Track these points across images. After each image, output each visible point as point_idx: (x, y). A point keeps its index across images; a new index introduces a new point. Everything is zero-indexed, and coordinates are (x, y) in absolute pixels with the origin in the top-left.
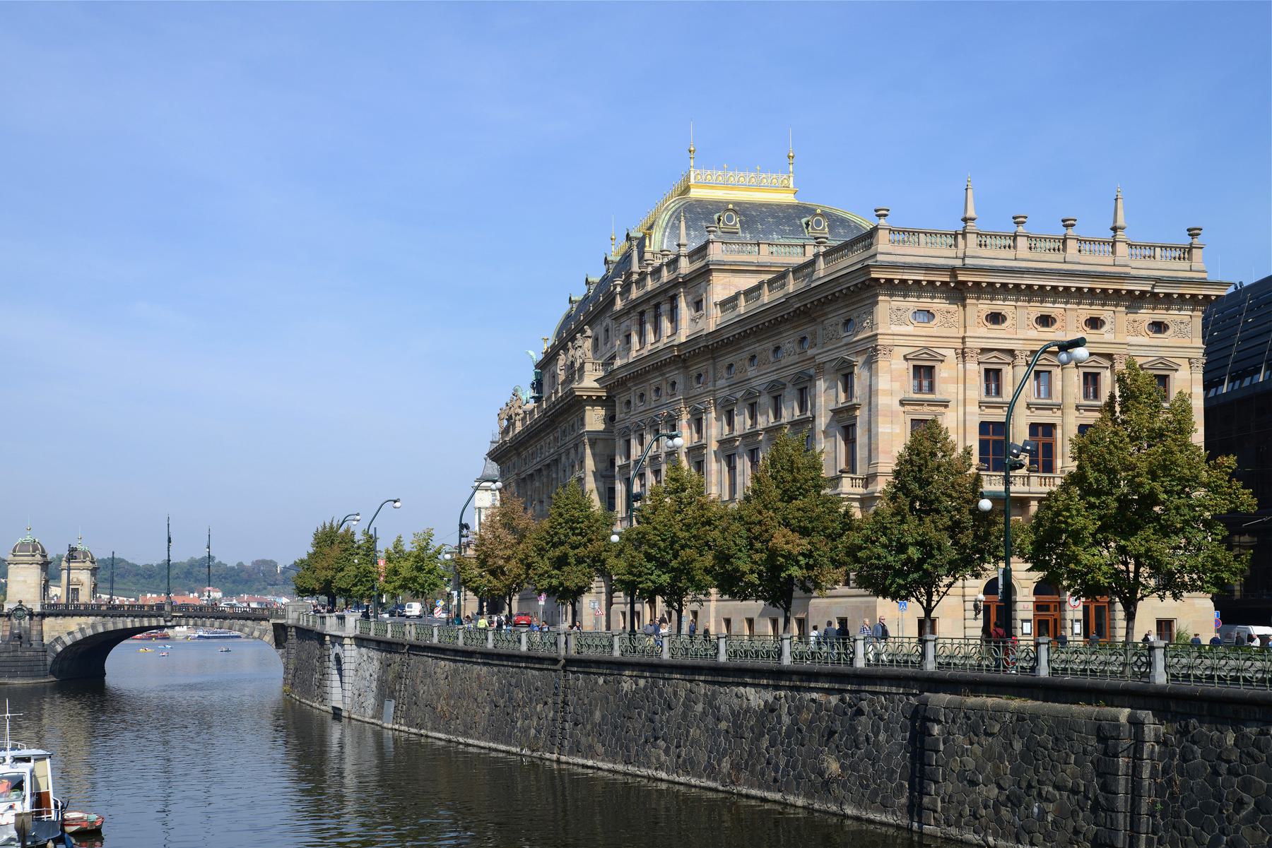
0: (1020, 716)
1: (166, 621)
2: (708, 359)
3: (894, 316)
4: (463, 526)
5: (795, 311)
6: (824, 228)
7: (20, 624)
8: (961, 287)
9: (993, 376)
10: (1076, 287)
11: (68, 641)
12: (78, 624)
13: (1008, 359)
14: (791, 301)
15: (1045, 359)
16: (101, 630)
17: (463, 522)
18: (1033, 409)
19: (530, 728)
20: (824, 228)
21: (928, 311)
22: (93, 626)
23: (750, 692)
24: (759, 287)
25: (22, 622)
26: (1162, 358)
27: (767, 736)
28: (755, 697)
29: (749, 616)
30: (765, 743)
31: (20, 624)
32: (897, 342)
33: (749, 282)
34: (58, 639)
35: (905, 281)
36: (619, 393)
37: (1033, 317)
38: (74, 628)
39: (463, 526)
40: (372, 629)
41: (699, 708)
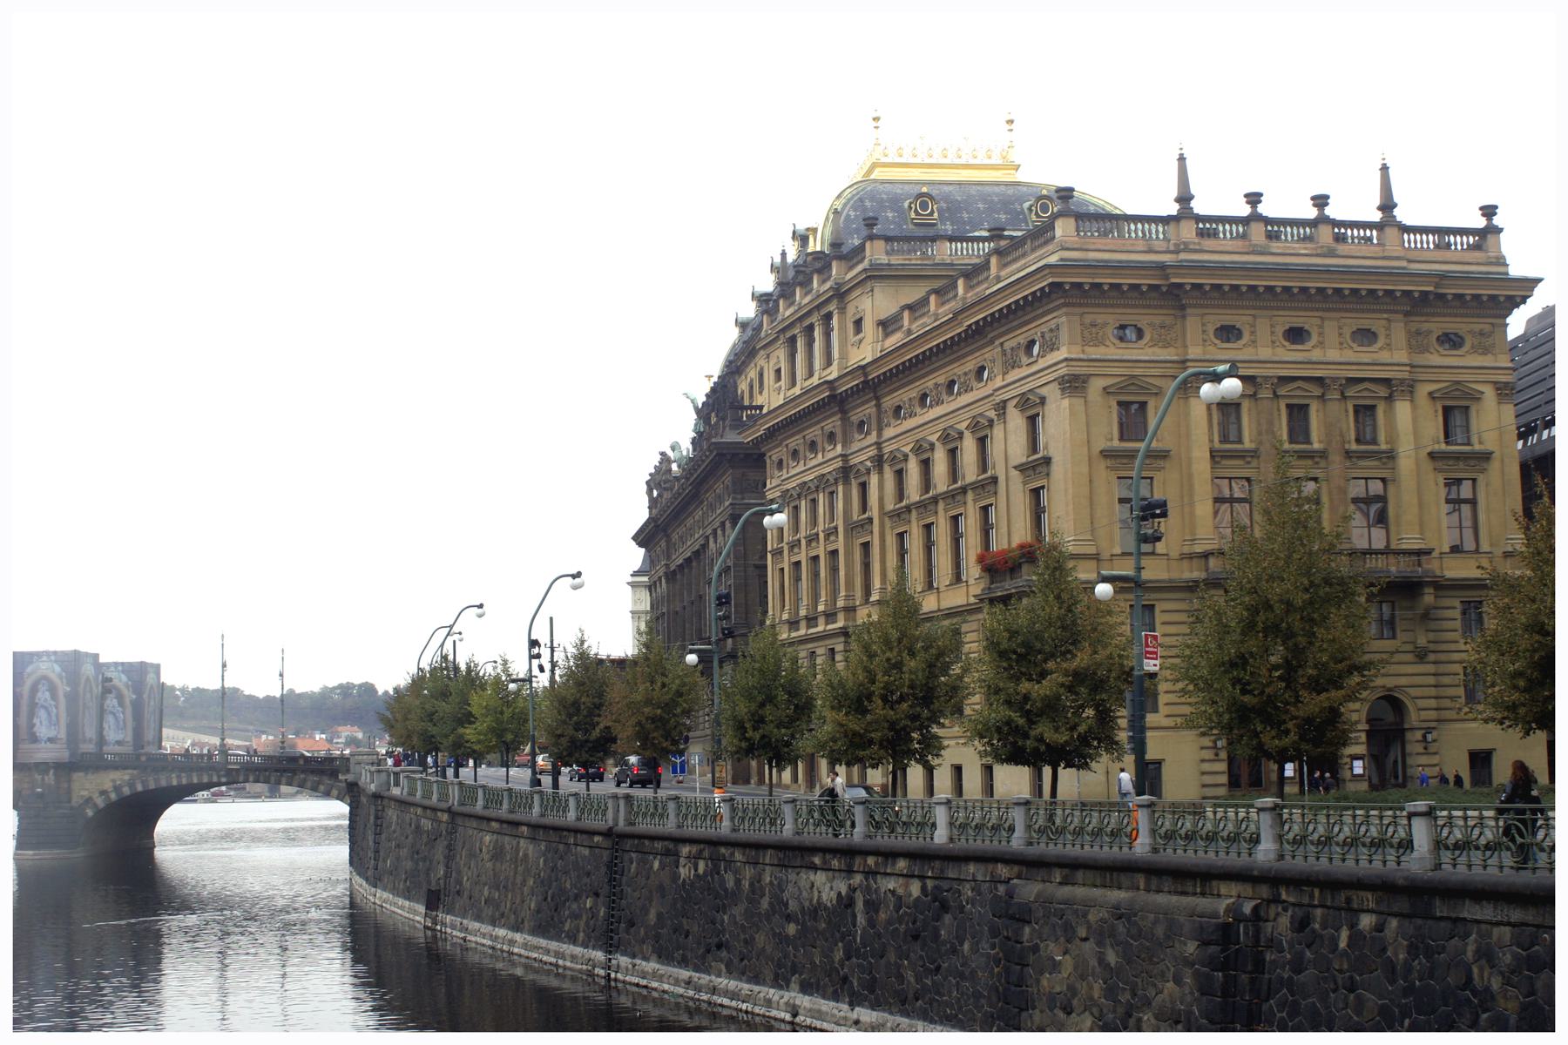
0: (1119, 913)
1: (219, 777)
2: (867, 402)
3: (1414, 342)
4: (534, 643)
5: (966, 331)
6: (932, 211)
7: (43, 779)
8: (1176, 292)
9: (1298, 413)
10: (1300, 287)
11: (100, 802)
12: (114, 781)
13: (1317, 392)
14: (960, 318)
15: (1366, 389)
16: (140, 788)
17: (533, 637)
18: (1354, 460)
19: (578, 932)
20: (932, 211)
21: (1369, 330)
22: (131, 785)
23: (820, 878)
24: (924, 302)
25: (46, 778)
26: (1458, 382)
27: (840, 944)
28: (825, 886)
29: (957, 762)
30: (839, 954)
31: (43, 779)
32: (1092, 371)
33: (912, 293)
34: (89, 800)
35: (1462, 296)
36: (770, 450)
37: (1280, 330)
38: (108, 786)
39: (534, 643)
40: (435, 792)
41: (765, 904)
